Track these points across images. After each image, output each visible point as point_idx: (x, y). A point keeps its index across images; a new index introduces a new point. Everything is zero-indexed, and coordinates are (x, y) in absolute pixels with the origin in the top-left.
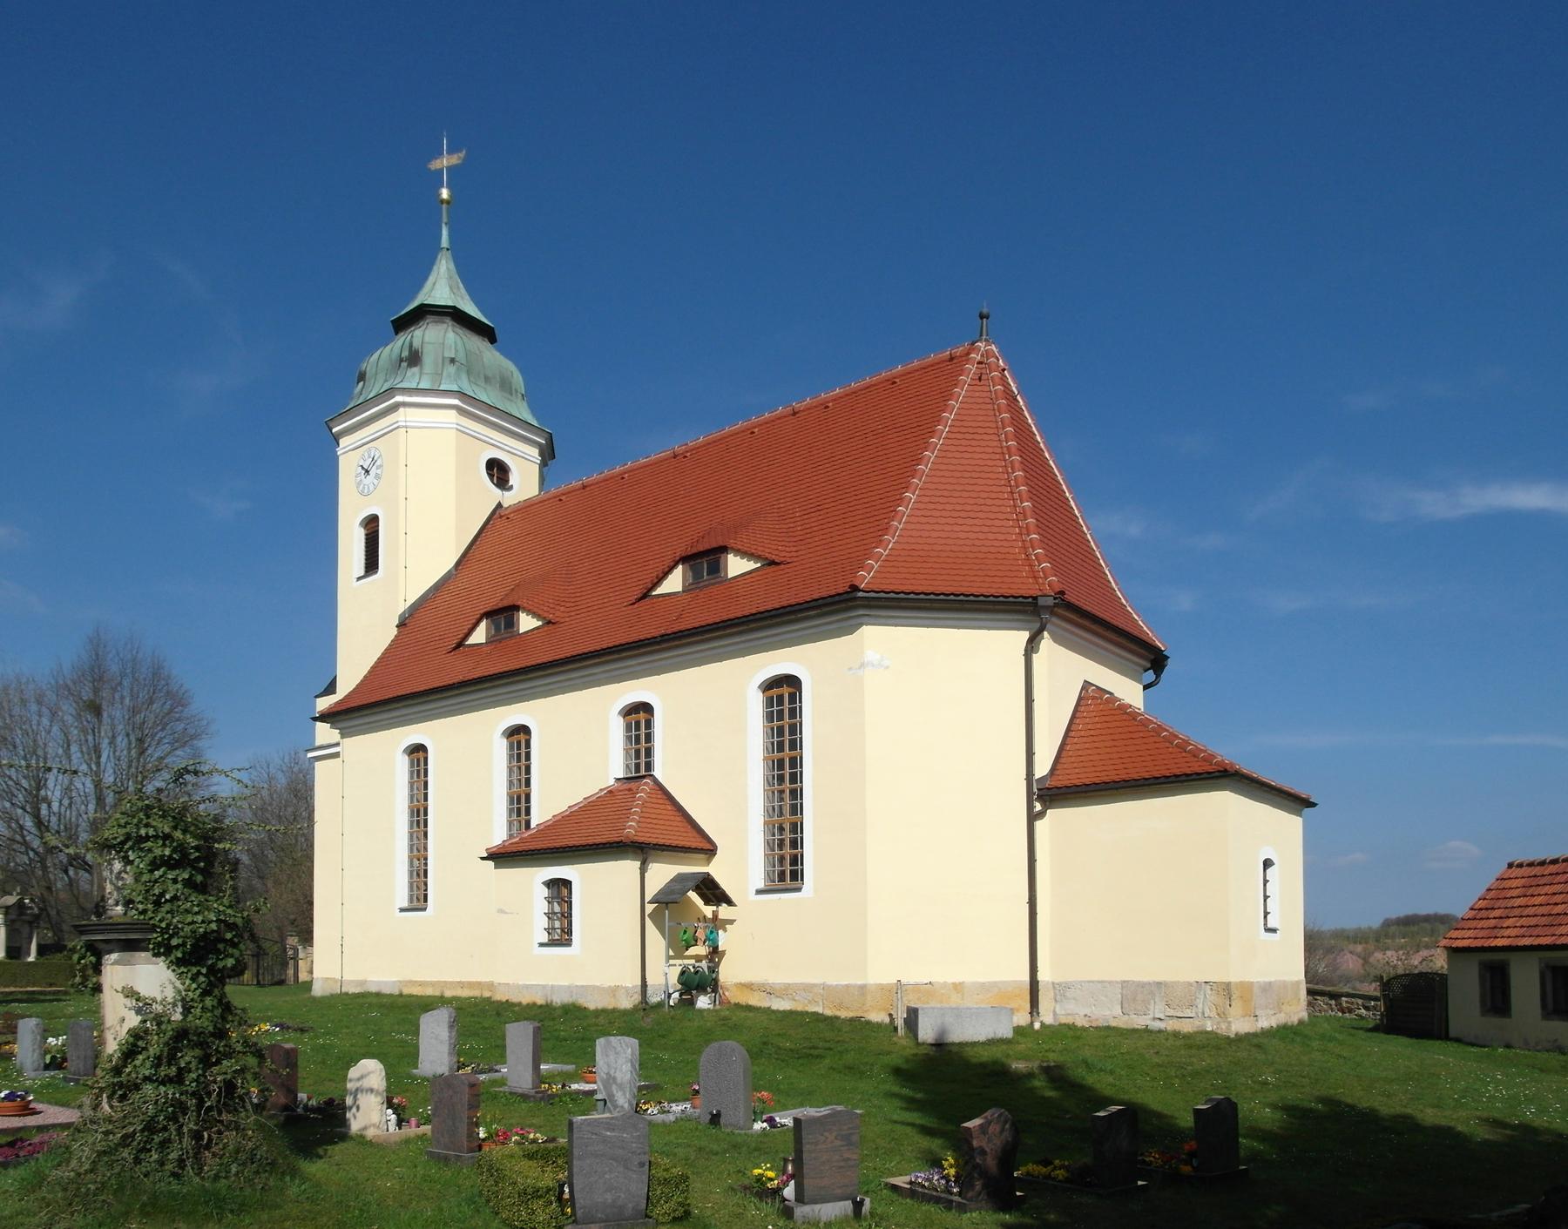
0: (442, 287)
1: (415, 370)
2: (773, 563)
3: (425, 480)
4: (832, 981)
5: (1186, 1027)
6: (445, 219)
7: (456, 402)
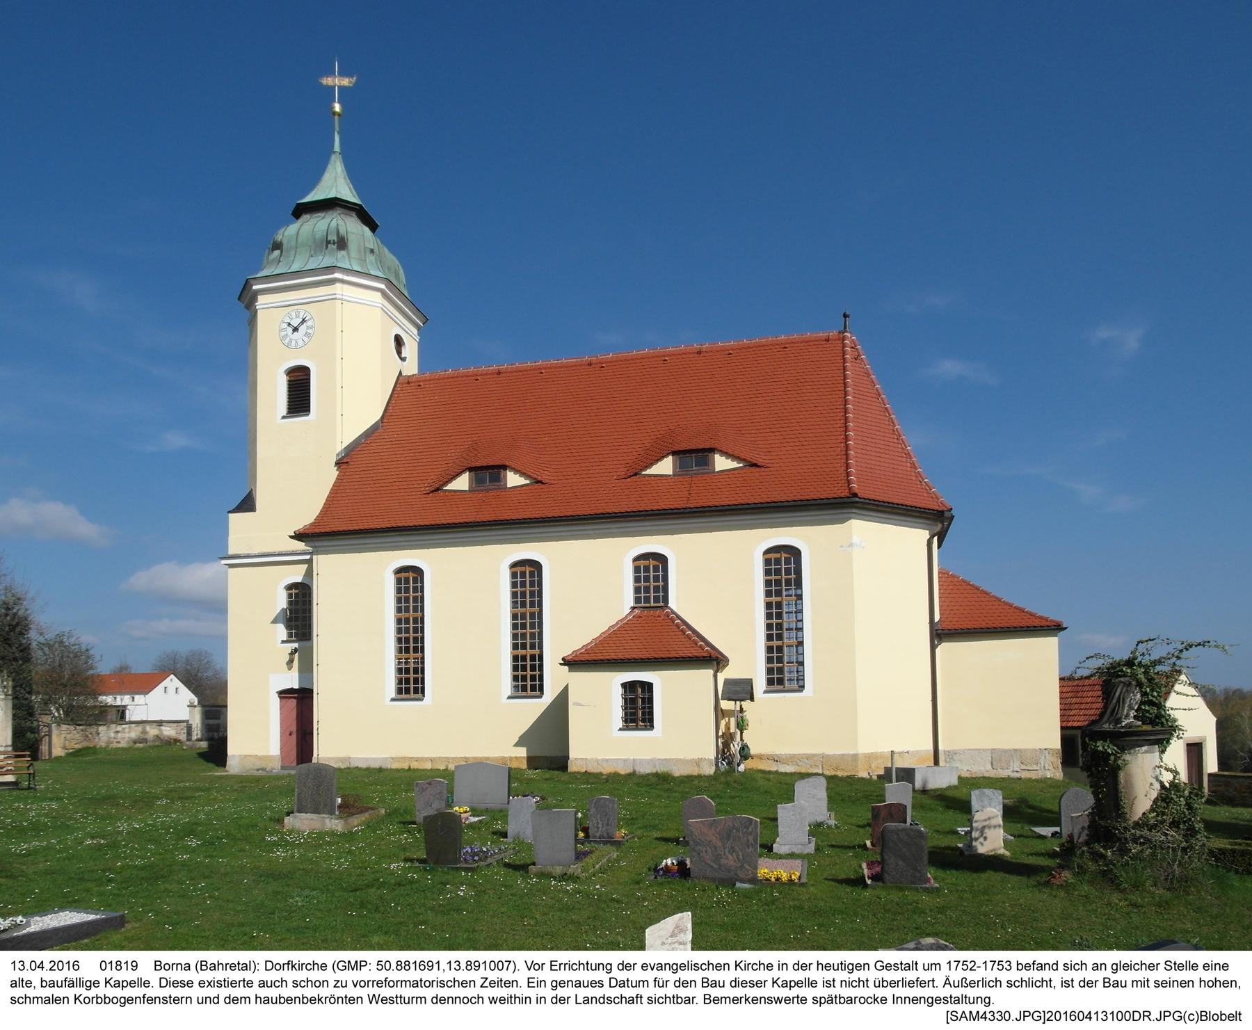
0: (335, 182)
1: (343, 253)
2: (756, 465)
4: (830, 751)
5: (1034, 776)
6: (337, 128)
7: (382, 286)
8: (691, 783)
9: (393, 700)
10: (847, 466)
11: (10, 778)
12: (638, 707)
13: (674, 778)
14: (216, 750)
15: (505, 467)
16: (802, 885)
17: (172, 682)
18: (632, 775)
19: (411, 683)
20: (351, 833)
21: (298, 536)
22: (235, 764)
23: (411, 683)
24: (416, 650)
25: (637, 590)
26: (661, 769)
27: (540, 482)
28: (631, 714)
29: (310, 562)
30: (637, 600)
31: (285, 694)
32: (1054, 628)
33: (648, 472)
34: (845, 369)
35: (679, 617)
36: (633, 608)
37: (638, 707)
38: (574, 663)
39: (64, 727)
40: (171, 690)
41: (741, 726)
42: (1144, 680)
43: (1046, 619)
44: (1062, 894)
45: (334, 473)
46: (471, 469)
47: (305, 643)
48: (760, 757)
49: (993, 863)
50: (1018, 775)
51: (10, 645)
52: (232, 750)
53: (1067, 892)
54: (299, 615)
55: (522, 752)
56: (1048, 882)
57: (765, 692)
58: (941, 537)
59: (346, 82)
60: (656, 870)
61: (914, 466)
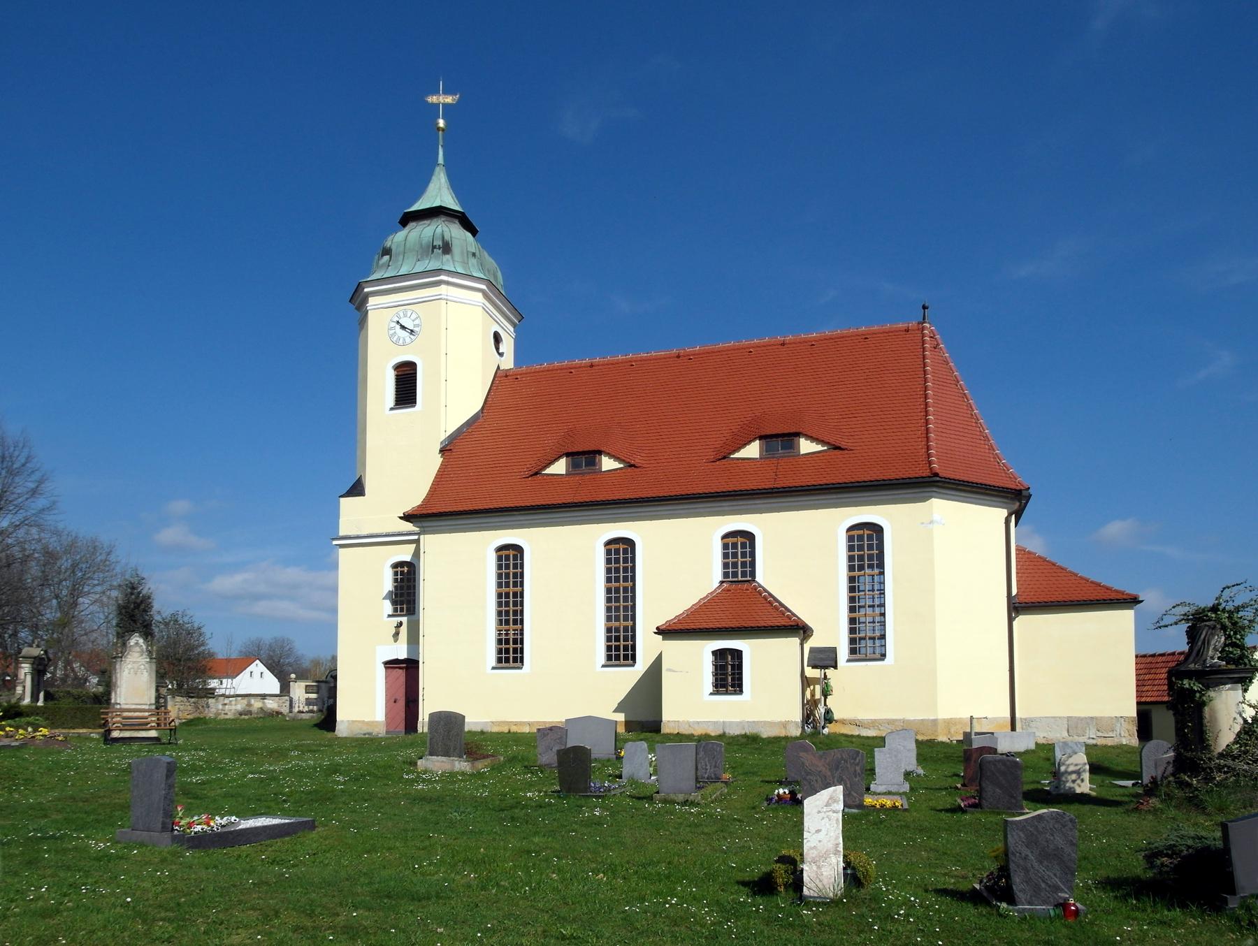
0: (439, 193)
1: (448, 257)
3: (445, 339)
5: (1109, 742)
7: (484, 287)
8: (778, 744)
9: (494, 668)
10: (928, 448)
11: (153, 734)
12: (728, 674)
13: (763, 740)
14: (328, 720)
15: (600, 453)
16: (906, 810)
17: (258, 667)
18: (722, 736)
19: (510, 652)
20: (479, 773)
21: (407, 517)
22: (342, 729)
23: (510, 652)
24: (515, 622)
25: (725, 566)
26: (748, 731)
27: (633, 466)
28: (722, 680)
29: (417, 542)
30: (726, 575)
31: (391, 664)
32: (1130, 601)
33: (736, 455)
34: (924, 357)
35: (765, 591)
36: (722, 582)
37: (728, 674)
38: (667, 632)
39: (178, 699)
40: (256, 675)
41: (826, 694)
42: (1228, 623)
43: (1123, 593)
44: (1151, 817)
45: (438, 460)
46: (568, 455)
47: (413, 617)
48: (843, 722)
49: (1083, 799)
50: (1094, 742)
51: (135, 621)
52: (340, 716)
53: (1155, 814)
54: (405, 591)
55: (621, 717)
56: (1137, 809)
57: (849, 661)
58: (1018, 514)
59: (449, 100)
60: (769, 800)
61: (991, 448)
